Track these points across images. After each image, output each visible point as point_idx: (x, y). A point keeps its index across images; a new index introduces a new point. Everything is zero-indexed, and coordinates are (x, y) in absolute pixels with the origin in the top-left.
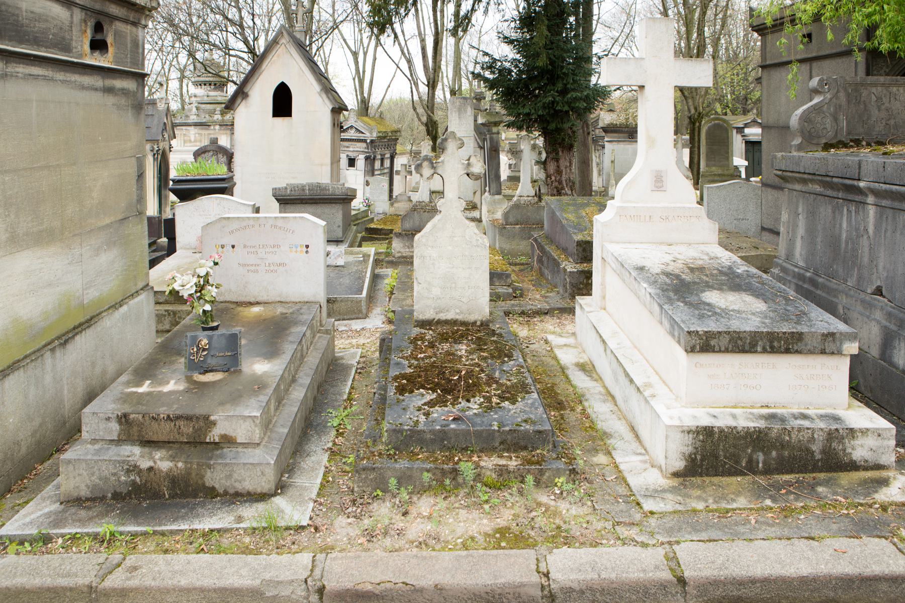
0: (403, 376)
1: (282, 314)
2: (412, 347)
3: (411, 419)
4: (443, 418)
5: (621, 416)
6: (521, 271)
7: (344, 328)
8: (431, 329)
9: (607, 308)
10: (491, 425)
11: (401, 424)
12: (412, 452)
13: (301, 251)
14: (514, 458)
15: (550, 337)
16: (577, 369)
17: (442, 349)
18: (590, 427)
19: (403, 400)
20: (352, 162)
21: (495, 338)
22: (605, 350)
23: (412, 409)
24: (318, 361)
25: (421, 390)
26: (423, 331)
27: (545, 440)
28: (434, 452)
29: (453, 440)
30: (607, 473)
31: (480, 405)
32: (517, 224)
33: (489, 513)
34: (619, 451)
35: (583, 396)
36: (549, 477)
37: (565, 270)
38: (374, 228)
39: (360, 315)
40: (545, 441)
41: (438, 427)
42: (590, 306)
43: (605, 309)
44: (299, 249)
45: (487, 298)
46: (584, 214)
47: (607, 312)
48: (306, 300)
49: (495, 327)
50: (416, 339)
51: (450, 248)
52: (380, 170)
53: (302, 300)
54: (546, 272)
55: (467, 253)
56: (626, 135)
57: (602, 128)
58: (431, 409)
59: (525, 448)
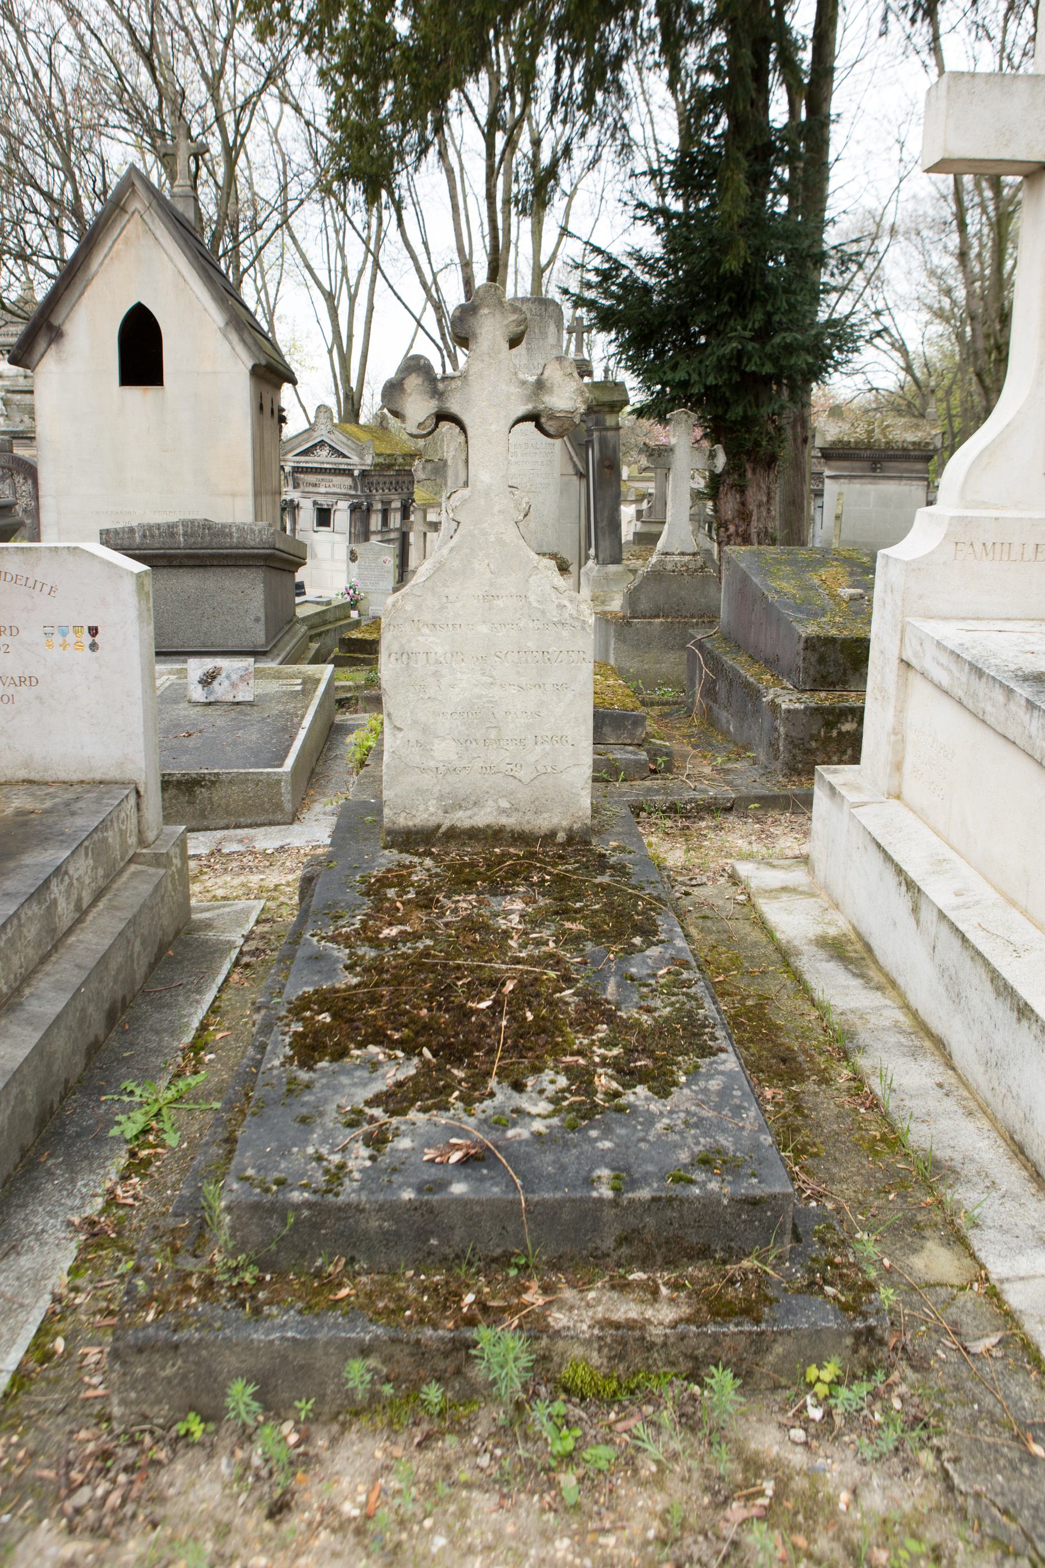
0: (324, 1000)
1: (20, 813)
2: (368, 903)
3: (320, 1158)
4: (430, 1154)
5: (972, 1105)
6: (663, 716)
7: (235, 847)
8: (430, 854)
9: (906, 793)
10: (590, 1182)
11: (280, 1182)
12: (318, 1274)
13: (78, 644)
14: (664, 1291)
15: (744, 869)
16: (822, 954)
17: (455, 911)
18: (884, 1139)
19: (308, 1086)
20: (324, 517)
21: (604, 879)
22: (915, 910)
23: (331, 1118)
24: (107, 942)
25: (372, 1049)
26: (407, 858)
27: (771, 1227)
28: (393, 1271)
29: (459, 1234)
30: (969, 1325)
31: (555, 1100)
32: (658, 616)
33: (577, 1507)
34: (990, 1234)
35: (851, 1035)
36: (784, 1358)
37: (774, 706)
38: (357, 640)
39: (279, 817)
40: (767, 1232)
41: (408, 1195)
42: (858, 788)
43: (898, 797)
44: (71, 638)
45: (587, 772)
46: (816, 581)
47: (907, 805)
48: (98, 776)
49: (608, 846)
50: (383, 882)
51: (484, 629)
52: (381, 532)
53: (88, 777)
54: (724, 715)
55: (531, 645)
56: (866, 464)
57: (821, 449)
58: (395, 1120)
59: (704, 1253)
